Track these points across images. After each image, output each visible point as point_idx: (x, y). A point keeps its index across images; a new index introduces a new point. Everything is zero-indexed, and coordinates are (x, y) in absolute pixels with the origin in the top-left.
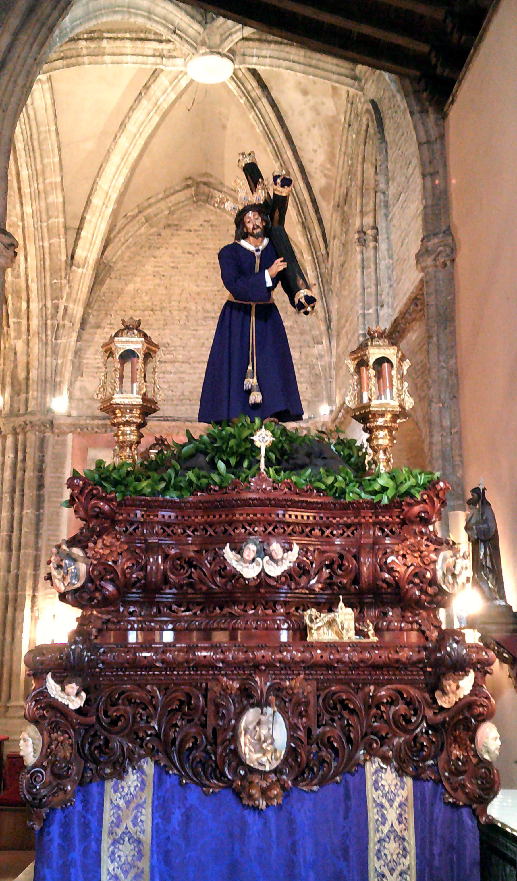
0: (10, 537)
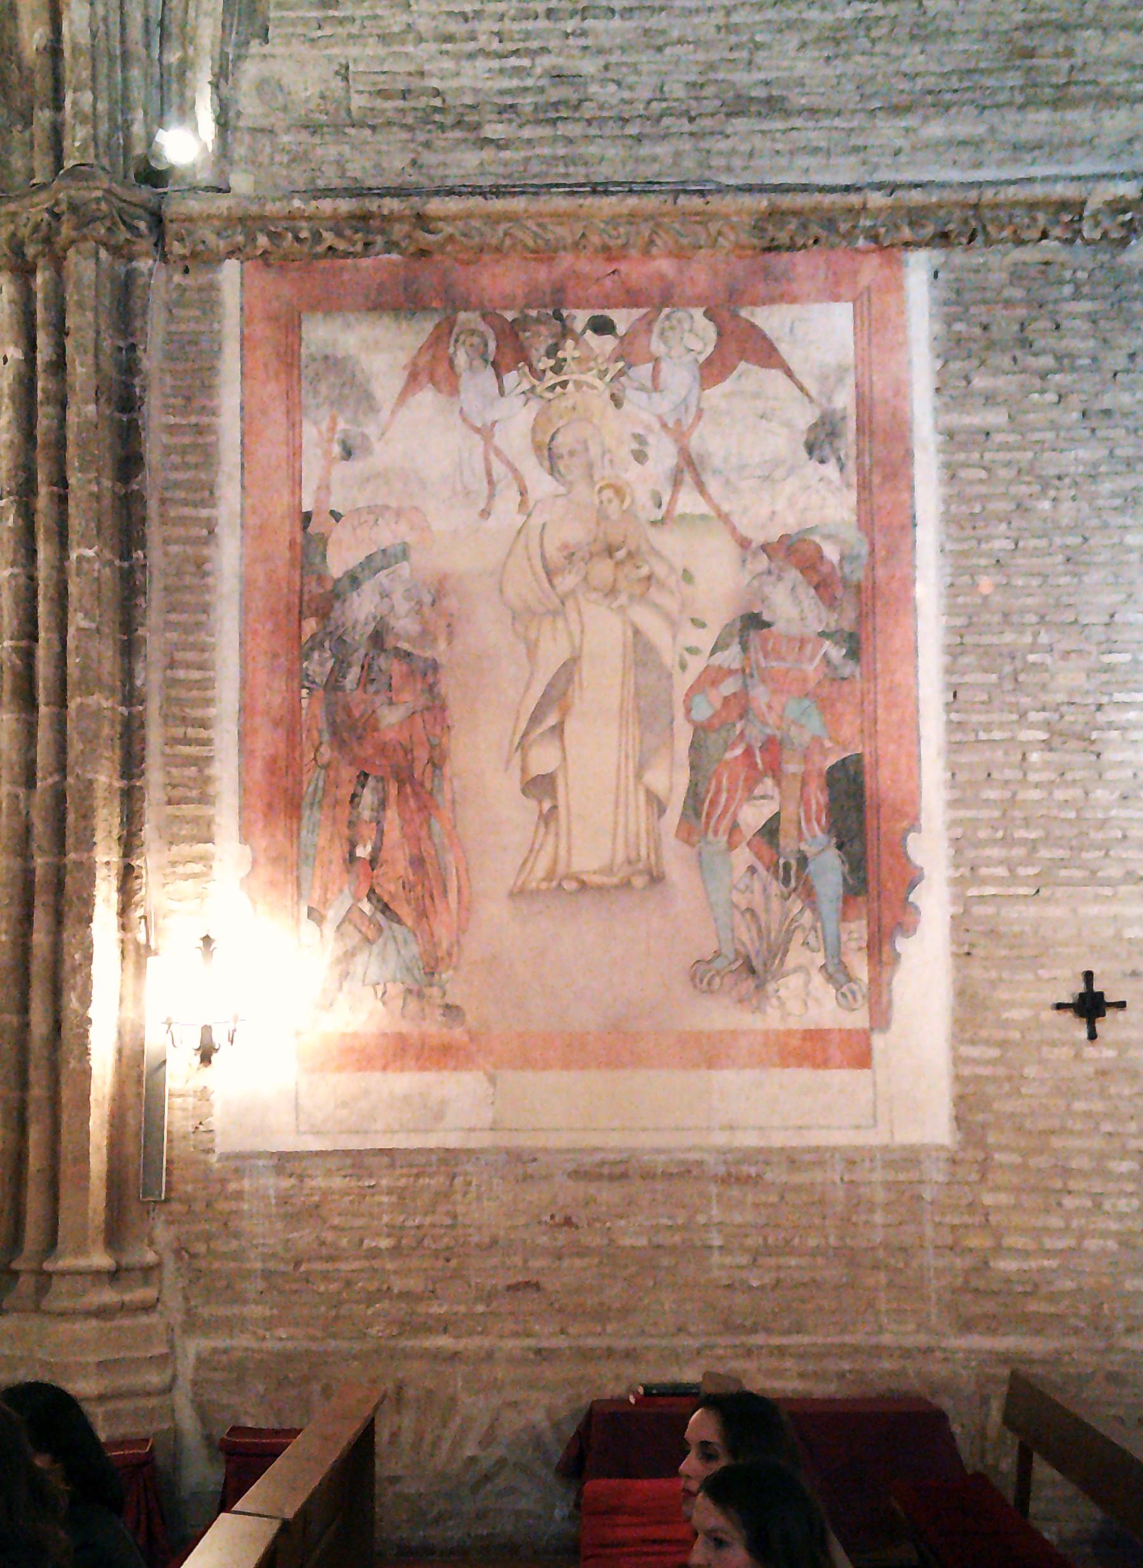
0: (28, 656)
